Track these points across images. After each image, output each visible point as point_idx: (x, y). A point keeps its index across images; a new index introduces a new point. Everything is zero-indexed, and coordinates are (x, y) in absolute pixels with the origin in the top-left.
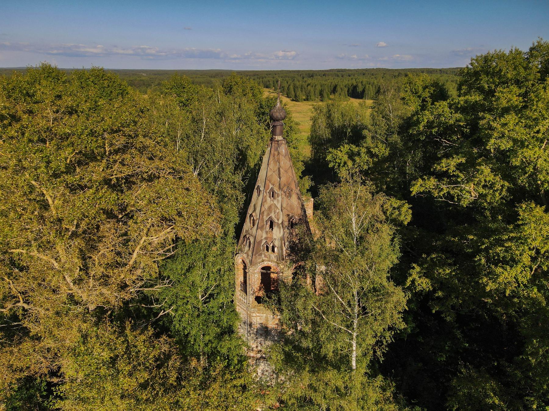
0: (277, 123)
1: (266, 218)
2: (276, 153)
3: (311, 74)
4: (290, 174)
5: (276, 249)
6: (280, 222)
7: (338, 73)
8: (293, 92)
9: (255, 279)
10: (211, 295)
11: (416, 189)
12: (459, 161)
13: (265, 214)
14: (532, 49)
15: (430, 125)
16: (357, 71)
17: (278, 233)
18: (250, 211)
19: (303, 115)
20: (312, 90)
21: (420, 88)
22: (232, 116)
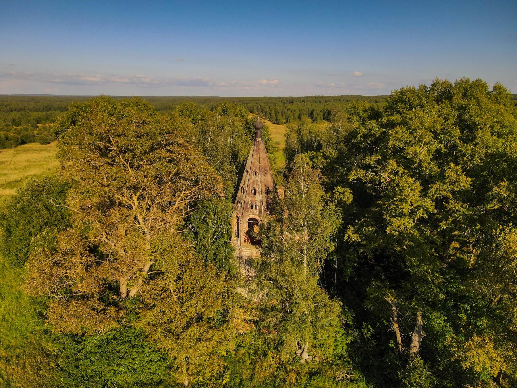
0: (258, 131)
1: (251, 188)
2: (258, 149)
3: (291, 101)
4: (266, 161)
5: (257, 207)
6: (260, 190)
7: (316, 99)
8: (274, 116)
9: (244, 226)
10: (218, 237)
11: (352, 177)
12: (378, 158)
13: (251, 185)
14: (432, 85)
15: (366, 136)
16: (333, 97)
17: (258, 197)
18: (241, 185)
19: (278, 133)
20: (291, 114)
21: (361, 111)
22: (228, 129)
